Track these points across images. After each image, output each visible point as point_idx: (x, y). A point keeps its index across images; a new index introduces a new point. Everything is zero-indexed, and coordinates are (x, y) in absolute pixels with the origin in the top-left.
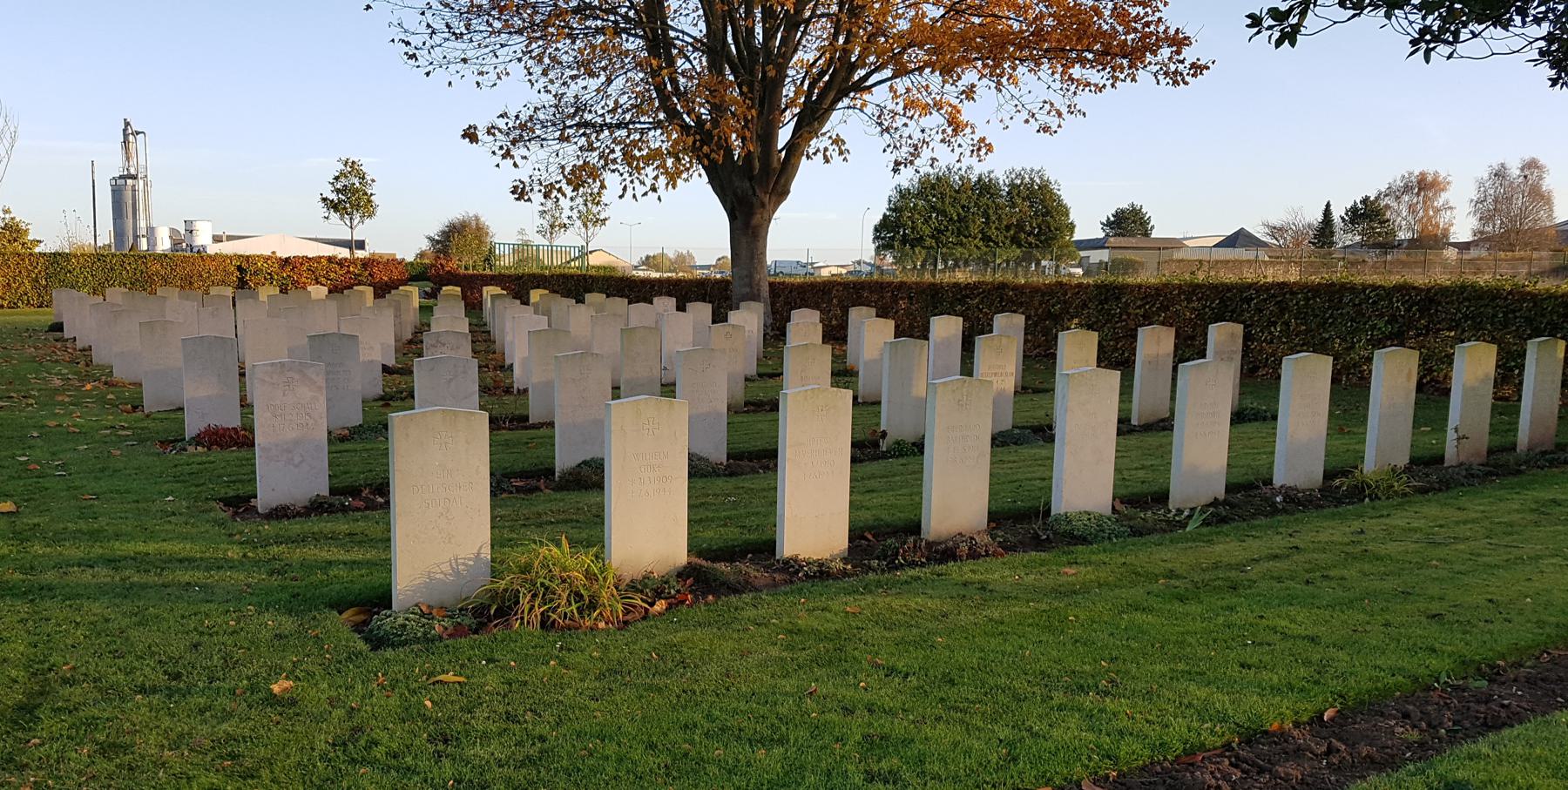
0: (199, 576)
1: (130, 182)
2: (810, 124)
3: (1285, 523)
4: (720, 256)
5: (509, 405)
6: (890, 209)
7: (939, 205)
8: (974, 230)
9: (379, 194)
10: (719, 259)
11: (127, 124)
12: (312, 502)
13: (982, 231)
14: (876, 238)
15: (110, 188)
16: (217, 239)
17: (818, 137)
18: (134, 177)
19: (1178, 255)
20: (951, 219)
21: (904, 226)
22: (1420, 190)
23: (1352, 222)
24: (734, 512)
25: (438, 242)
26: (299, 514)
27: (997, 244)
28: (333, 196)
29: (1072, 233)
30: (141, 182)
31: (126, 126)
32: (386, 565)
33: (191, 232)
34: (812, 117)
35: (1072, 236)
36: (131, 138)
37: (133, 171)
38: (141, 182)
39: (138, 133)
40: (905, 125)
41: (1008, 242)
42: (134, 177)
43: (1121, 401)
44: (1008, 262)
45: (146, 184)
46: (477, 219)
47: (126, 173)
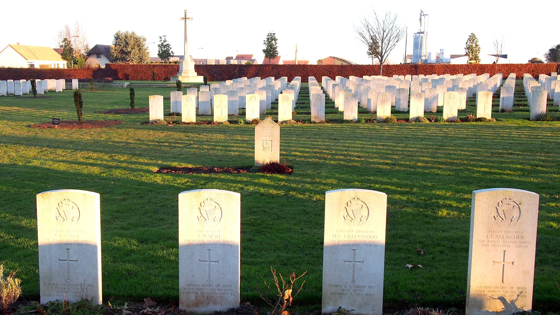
0: (498, 133)
1: (421, 35)
3: (61, 185)
11: (422, 12)
12: (96, 47)
15: (413, 37)
18: (422, 33)
24: (492, 140)
26: (428, 113)
29: (530, 312)
30: (425, 34)
31: (421, 13)
32: (409, 117)
36: (423, 17)
37: (422, 31)
38: (425, 34)
40: (119, 191)
42: (422, 33)
43: (409, 109)
45: (427, 35)
47: (419, 31)
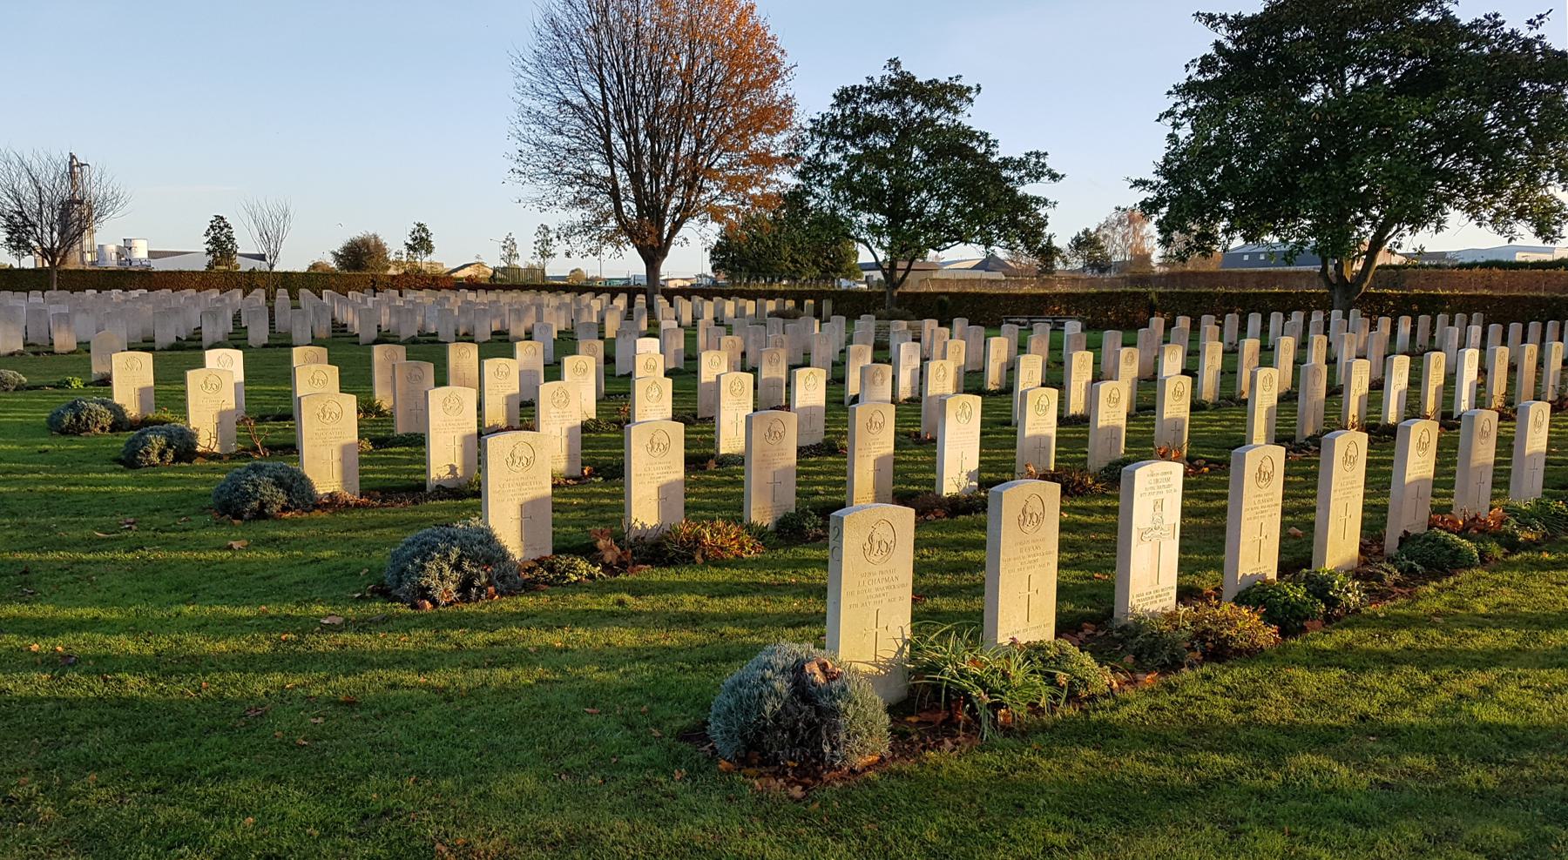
2: (827, 508)
4: (574, 268)
5: (602, 335)
6: (721, 237)
7: (759, 235)
8: (785, 254)
9: (434, 240)
10: (572, 271)
11: (73, 157)
13: (790, 255)
14: (712, 259)
16: (152, 254)
17: (906, 642)
19: (936, 275)
20: (768, 246)
21: (732, 250)
22: (1130, 222)
23: (1077, 248)
25: (341, 256)
27: (802, 265)
28: (411, 242)
29: (857, 258)
33: (130, 249)
34: (677, 226)
35: (856, 259)
39: (82, 165)
41: (810, 264)
44: (811, 279)
46: (376, 237)
